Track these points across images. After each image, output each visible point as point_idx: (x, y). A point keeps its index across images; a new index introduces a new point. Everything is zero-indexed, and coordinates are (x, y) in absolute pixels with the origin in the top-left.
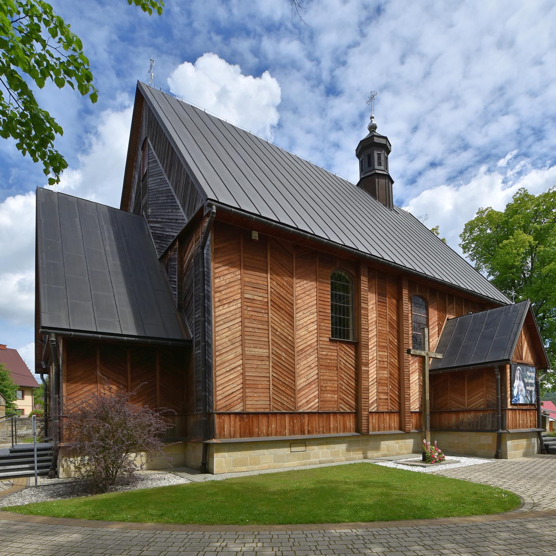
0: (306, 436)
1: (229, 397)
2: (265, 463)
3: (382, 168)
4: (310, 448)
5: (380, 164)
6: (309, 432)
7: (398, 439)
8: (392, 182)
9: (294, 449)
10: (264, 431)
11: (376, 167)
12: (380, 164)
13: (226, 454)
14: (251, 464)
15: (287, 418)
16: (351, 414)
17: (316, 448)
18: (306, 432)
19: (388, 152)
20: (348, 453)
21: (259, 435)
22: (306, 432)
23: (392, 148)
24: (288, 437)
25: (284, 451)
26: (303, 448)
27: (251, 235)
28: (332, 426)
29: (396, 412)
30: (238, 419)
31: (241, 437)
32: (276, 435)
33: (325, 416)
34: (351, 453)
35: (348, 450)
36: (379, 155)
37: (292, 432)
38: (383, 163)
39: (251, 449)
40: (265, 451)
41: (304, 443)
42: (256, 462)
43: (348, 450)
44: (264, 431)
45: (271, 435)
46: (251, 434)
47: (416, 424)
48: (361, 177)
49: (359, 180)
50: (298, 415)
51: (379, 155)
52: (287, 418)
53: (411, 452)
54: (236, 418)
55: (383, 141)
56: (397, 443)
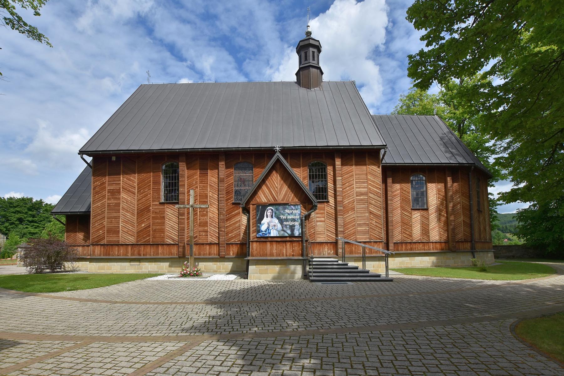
0: (142, 257)
1: (99, 237)
2: (114, 270)
3: (315, 62)
4: (141, 263)
5: (314, 59)
6: (144, 255)
7: (217, 261)
8: (322, 73)
9: (132, 263)
10: (116, 253)
11: (311, 61)
12: (314, 59)
13: (95, 264)
14: (107, 270)
15: (130, 248)
16: (416, 244)
17: (147, 263)
18: (142, 255)
19: (319, 51)
20: (170, 268)
21: (113, 256)
22: (142, 255)
23: (322, 49)
24: (130, 257)
25: (127, 264)
26: (138, 263)
27: (116, 159)
28: (160, 252)
29: (470, 242)
30: (102, 247)
31: (103, 256)
32: (123, 255)
33: (155, 246)
34: (173, 268)
35: (170, 266)
36: (313, 52)
37: (132, 255)
38: (316, 59)
39: (108, 262)
40: (115, 264)
41: (139, 260)
42: (103, 268)
43: (170, 266)
44: (116, 253)
45: (120, 256)
46: (109, 255)
47: (237, 252)
48: (301, 67)
49: (298, 69)
50: (136, 246)
51: (313, 52)
52: (130, 248)
53: (229, 270)
54: (101, 247)
55: (317, 44)
56: (215, 264)
